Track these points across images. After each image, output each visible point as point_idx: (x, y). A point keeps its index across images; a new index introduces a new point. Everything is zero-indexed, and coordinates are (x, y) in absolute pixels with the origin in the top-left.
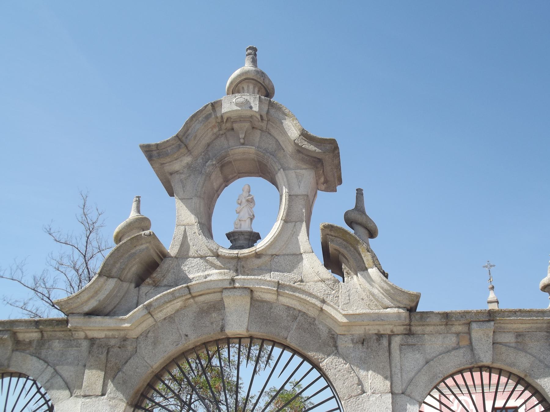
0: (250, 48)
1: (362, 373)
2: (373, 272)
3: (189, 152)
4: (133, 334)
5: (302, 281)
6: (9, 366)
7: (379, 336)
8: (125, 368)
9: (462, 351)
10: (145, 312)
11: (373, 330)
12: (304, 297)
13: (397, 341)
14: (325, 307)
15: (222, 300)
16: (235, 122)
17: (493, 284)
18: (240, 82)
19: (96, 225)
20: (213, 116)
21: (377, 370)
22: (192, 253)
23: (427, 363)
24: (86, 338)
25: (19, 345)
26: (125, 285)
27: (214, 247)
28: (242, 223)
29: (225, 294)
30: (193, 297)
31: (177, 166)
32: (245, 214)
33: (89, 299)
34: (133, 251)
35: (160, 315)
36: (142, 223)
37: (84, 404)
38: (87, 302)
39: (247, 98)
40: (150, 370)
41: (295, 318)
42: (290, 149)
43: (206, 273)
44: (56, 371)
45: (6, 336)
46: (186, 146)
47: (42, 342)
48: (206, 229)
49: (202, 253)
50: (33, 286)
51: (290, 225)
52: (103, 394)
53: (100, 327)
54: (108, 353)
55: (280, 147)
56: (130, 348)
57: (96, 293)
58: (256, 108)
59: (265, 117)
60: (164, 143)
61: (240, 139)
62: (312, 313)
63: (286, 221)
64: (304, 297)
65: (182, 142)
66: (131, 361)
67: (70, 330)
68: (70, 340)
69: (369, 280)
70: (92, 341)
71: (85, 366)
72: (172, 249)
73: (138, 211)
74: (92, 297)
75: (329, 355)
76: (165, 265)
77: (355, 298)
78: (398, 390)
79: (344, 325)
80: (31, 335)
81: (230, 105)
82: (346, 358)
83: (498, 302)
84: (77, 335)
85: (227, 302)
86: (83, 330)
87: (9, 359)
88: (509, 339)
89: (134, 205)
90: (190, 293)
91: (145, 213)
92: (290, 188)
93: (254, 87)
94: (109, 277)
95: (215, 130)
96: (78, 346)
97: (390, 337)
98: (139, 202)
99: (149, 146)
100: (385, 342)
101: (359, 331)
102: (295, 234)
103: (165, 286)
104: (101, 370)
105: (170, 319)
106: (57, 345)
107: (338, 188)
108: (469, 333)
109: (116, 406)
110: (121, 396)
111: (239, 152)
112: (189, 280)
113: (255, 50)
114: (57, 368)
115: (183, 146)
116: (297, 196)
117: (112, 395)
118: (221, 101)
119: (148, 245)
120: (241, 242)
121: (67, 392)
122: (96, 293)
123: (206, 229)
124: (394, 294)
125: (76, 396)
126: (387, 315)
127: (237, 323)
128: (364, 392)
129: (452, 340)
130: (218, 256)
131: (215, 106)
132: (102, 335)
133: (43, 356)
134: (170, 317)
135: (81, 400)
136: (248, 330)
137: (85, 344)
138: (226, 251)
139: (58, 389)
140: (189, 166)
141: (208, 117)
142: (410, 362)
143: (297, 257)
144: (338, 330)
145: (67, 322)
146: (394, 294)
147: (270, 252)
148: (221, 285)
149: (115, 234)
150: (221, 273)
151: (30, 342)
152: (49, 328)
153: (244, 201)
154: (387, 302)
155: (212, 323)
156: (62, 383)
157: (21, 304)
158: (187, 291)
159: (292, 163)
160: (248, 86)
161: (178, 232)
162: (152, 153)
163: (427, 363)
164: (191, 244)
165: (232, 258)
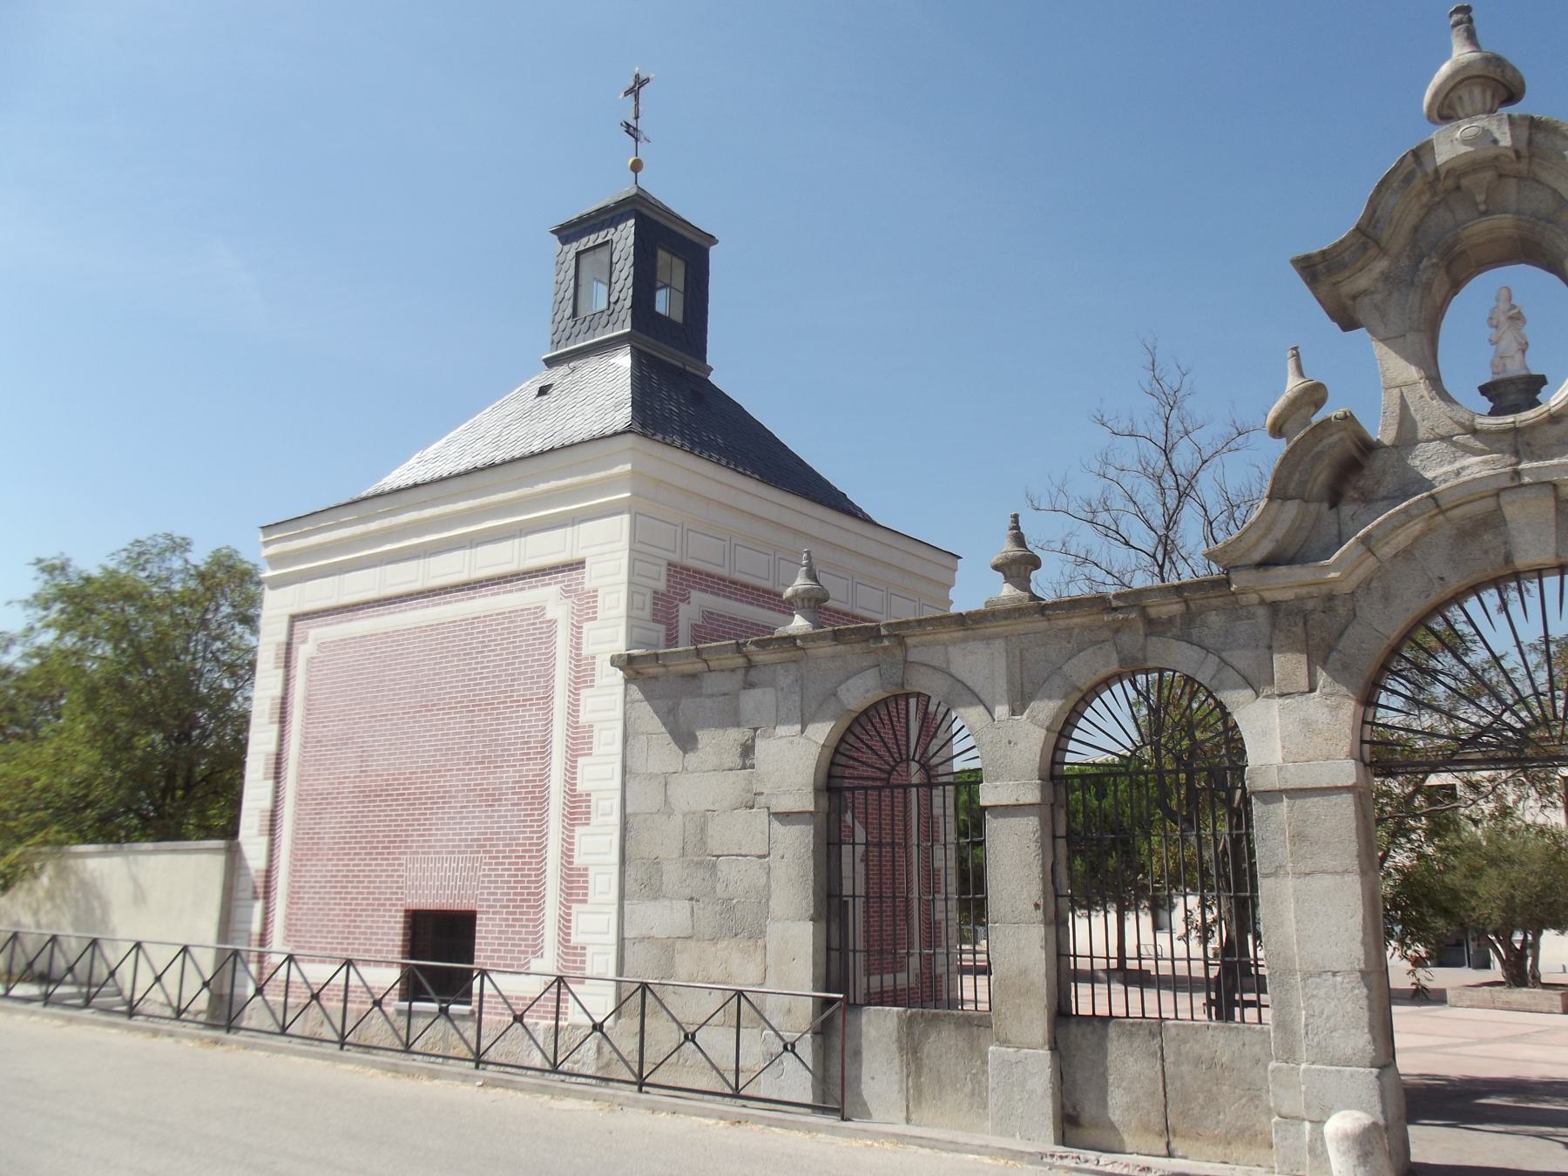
0: (1457, 11)
3: (1383, 251)
4: (1346, 587)
6: (1145, 660)
8: (1341, 646)
10: (1362, 548)
15: (1499, 507)
16: (1464, 174)
18: (1453, 88)
19: (1179, 394)
20: (1419, 174)
22: (1422, 433)
24: (1262, 602)
25: (1154, 626)
26: (1313, 507)
27: (1464, 417)
28: (1508, 361)
31: (1363, 282)
32: (1509, 342)
33: (1258, 542)
34: (1319, 448)
35: (1386, 551)
36: (1314, 395)
37: (1282, 708)
39: (1483, 122)
40: (1387, 642)
43: (1457, 465)
45: (1133, 615)
46: (1377, 243)
47: (1189, 618)
49: (1442, 431)
52: (1312, 690)
53: (1285, 583)
54: (1305, 624)
56: (1342, 611)
57: (1269, 529)
58: (1505, 140)
59: (1525, 153)
60: (1335, 246)
61: (1477, 204)
65: (1368, 236)
66: (1350, 631)
67: (1233, 594)
68: (1235, 609)
70: (1274, 607)
71: (1270, 647)
72: (1382, 431)
73: (1300, 372)
74: (1263, 536)
76: (1378, 462)
80: (1170, 608)
81: (1451, 144)
84: (1244, 599)
85: (1509, 511)
86: (1255, 592)
87: (1144, 648)
89: (1291, 365)
90: (1438, 506)
93: (1484, 91)
95: (1425, 198)
98: (1297, 356)
99: (1307, 258)
103: (1384, 498)
104: (1300, 652)
105: (1406, 553)
106: (1214, 619)
109: (1338, 707)
110: (1344, 690)
112: (1428, 484)
113: (1466, 10)
114: (1224, 655)
115: (1371, 244)
117: (1328, 690)
119: (1342, 434)
120: (1512, 398)
121: (1250, 692)
122: (1269, 529)
125: (1267, 697)
130: (1474, 432)
131: (1420, 154)
132: (1289, 595)
133: (1195, 638)
134: (1405, 551)
135: (1276, 703)
136: (1557, 556)
137: (1262, 612)
139: (1234, 688)
140: (1385, 277)
141: (1408, 179)
145: (1228, 582)
148: (1495, 485)
149: (1269, 421)
150: (1485, 462)
151: (1171, 620)
153: (1503, 318)
155: (1486, 552)
158: (1431, 503)
160: (1471, 92)
161: (1389, 401)
162: (1312, 269)
164: (1418, 418)
165: (1504, 432)
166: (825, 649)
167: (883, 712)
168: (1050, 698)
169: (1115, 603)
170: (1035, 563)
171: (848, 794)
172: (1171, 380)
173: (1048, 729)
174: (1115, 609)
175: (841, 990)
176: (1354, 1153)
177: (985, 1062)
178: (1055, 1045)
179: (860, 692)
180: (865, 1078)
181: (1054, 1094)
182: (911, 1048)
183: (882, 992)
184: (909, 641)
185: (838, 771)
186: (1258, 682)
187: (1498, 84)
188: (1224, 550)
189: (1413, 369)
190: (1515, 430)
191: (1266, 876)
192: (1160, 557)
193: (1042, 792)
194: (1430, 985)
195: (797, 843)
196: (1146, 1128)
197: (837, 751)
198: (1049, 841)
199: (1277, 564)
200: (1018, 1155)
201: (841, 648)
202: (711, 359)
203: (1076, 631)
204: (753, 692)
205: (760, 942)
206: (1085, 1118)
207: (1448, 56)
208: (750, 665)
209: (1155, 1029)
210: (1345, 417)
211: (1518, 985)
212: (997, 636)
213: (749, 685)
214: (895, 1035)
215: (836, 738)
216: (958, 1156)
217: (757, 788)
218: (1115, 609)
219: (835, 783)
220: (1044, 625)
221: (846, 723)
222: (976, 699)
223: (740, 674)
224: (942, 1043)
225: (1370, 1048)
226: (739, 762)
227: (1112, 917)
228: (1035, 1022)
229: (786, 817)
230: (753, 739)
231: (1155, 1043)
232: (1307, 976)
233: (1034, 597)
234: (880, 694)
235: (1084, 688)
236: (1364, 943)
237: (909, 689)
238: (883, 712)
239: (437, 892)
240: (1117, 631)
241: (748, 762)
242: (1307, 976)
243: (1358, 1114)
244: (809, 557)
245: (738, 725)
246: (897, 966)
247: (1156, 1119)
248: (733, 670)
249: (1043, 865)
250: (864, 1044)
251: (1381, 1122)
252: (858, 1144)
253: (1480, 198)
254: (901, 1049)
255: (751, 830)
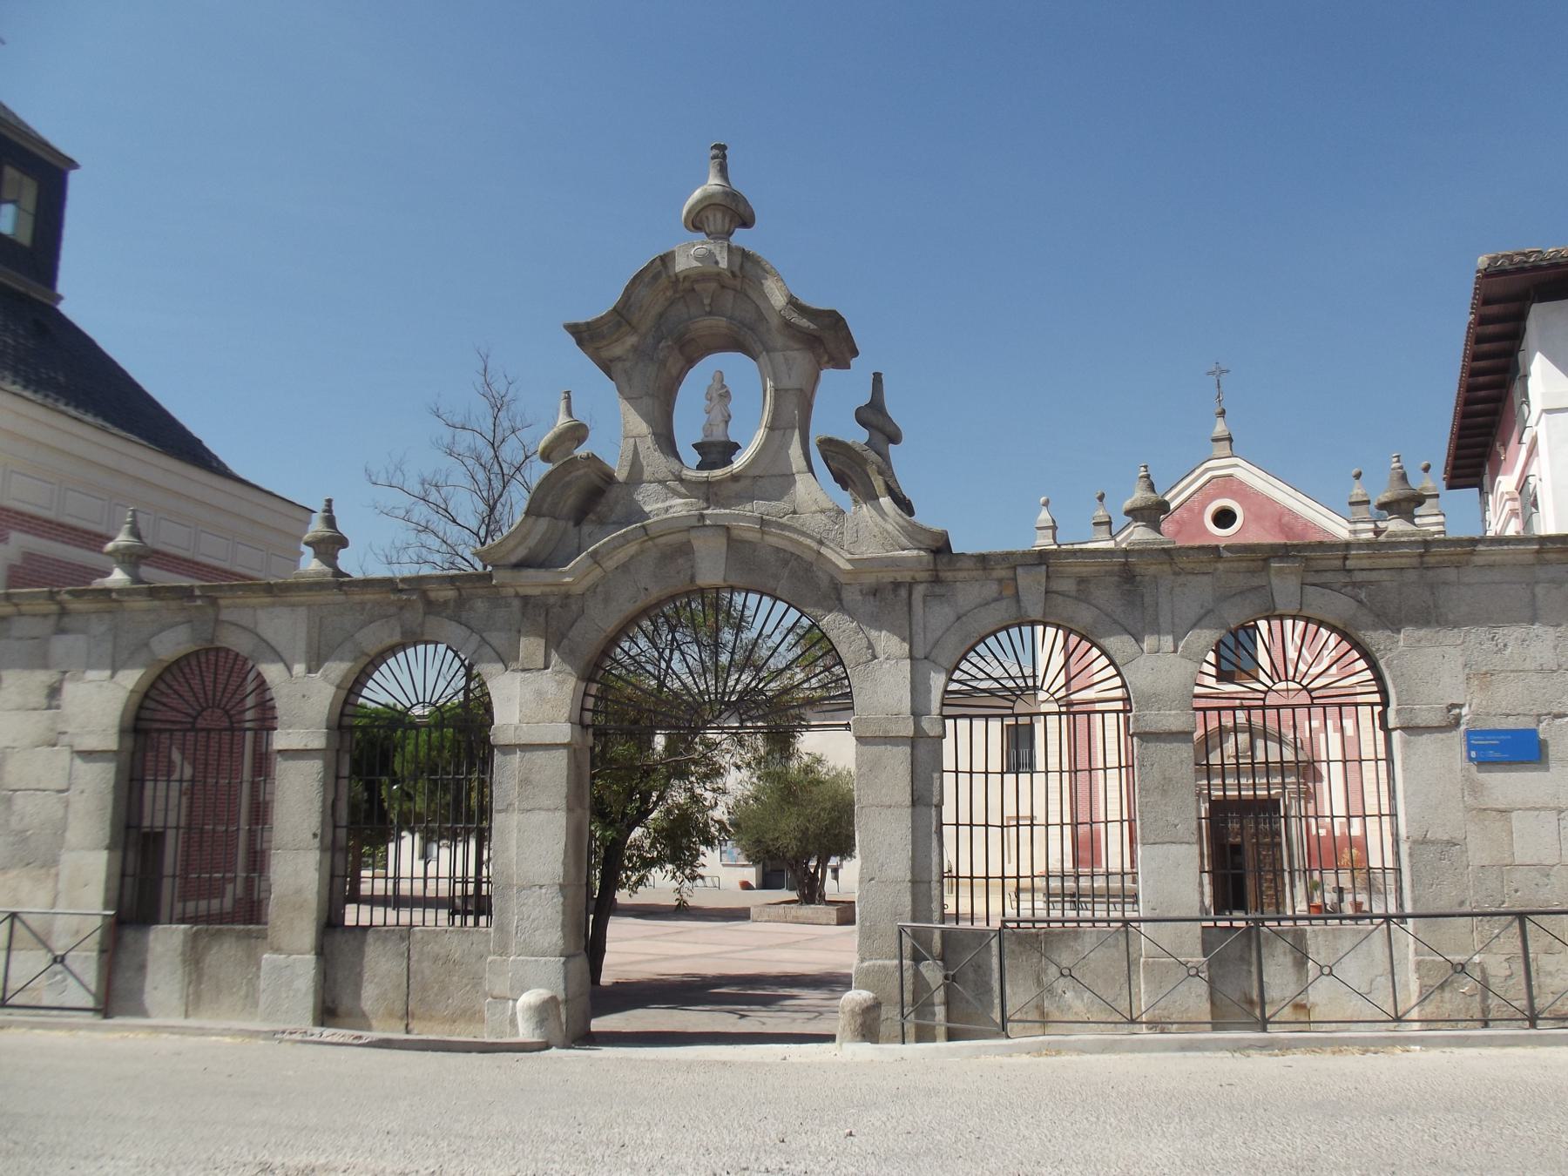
0: (715, 147)
1: (874, 634)
2: (885, 501)
4: (578, 590)
5: (794, 512)
7: (896, 585)
8: (570, 634)
9: (1004, 603)
10: (590, 561)
11: (888, 577)
12: (795, 536)
13: (919, 591)
14: (823, 550)
16: (697, 281)
17: (1224, 405)
21: (893, 630)
23: (959, 618)
24: (517, 595)
25: (431, 606)
26: (561, 524)
29: (693, 534)
30: (652, 539)
31: (617, 350)
32: (717, 415)
33: (516, 547)
35: (610, 564)
36: (577, 433)
37: (523, 680)
38: (513, 550)
41: (786, 563)
42: (775, 322)
43: (668, 504)
44: (483, 638)
47: (461, 602)
48: (666, 442)
49: (660, 478)
50: (422, 494)
51: (778, 433)
52: (546, 667)
53: (534, 582)
55: (761, 317)
57: (524, 538)
58: (724, 264)
60: (597, 320)
62: (809, 556)
63: (772, 428)
64: (795, 536)
68: (497, 599)
69: (881, 511)
70: (526, 600)
72: (621, 474)
73: (569, 413)
74: (519, 544)
75: (830, 611)
76: (613, 493)
77: (864, 534)
78: (919, 654)
79: (848, 572)
82: (853, 616)
83: (1230, 439)
85: (698, 544)
87: (422, 625)
88: (1068, 586)
89: (563, 405)
91: (580, 415)
92: (775, 380)
94: (539, 515)
95: (669, 294)
96: (508, 605)
97: (911, 586)
98: (568, 399)
100: (903, 593)
101: (869, 579)
102: (786, 446)
105: (624, 567)
106: (480, 606)
107: (853, 362)
108: (1015, 579)
109: (564, 682)
110: (569, 669)
111: (705, 324)
112: (646, 516)
116: (786, 390)
118: (673, 252)
121: (500, 666)
122: (524, 538)
123: (666, 442)
124: (915, 534)
126: (904, 559)
127: (710, 570)
128: (875, 657)
129: (992, 589)
130: (681, 480)
131: (666, 259)
132: (537, 591)
135: (519, 675)
137: (516, 603)
138: (691, 474)
140: (635, 349)
141: (656, 277)
142: (938, 617)
143: (788, 479)
144: (842, 579)
145: (490, 576)
146: (915, 534)
147: (751, 473)
149: (542, 444)
151: (446, 603)
152: (468, 585)
154: (904, 541)
156: (493, 654)
157: (403, 513)
159: (779, 340)
162: (584, 335)
163: (959, 618)
165: (700, 483)
166: (142, 603)
167: (194, 662)
168: (341, 660)
169: (400, 586)
170: (342, 542)
171: (155, 735)
172: (499, 386)
173: (338, 687)
174: (401, 591)
175: (133, 909)
176: (534, 1020)
177: (259, 968)
178: (321, 951)
179: (172, 643)
180: (148, 987)
181: (316, 991)
182: (193, 959)
183: (209, 915)
184: (222, 602)
185: (146, 714)
186: (506, 659)
187: (731, 212)
188: (488, 551)
189: (645, 425)
190: (708, 483)
191: (499, 811)
192: (482, 533)
193: (328, 739)
194: (691, 902)
195: (97, 782)
196: (391, 1014)
197: (146, 696)
198: (332, 781)
199: (529, 566)
200: (255, 1034)
201: (157, 603)
202: (62, 287)
203: (369, 606)
204: (64, 637)
205: (53, 871)
206: (342, 1009)
207: (705, 182)
208: (63, 612)
209: (405, 934)
210: (588, 457)
211: (808, 903)
212: (301, 604)
213: (61, 631)
214: (180, 950)
215: (146, 685)
216: (203, 1038)
217: (61, 727)
218: (401, 591)
219: (141, 726)
220: (341, 598)
221: (157, 671)
222: (278, 657)
223: (52, 621)
224: (224, 953)
225: (561, 942)
226: (44, 702)
227: (473, 844)
228: (306, 932)
229: (88, 755)
230: (61, 681)
231: (404, 946)
232: (522, 888)
233: (338, 573)
234: (192, 648)
235: (372, 653)
236: (564, 864)
237: (218, 644)
238: (194, 662)
239: (1559, 737)
240: (401, 608)
241: (55, 703)
242: (522, 888)
243: (542, 991)
244: (134, 516)
245: (46, 667)
246: (215, 890)
247: (399, 1006)
248: (45, 616)
249: (324, 801)
250: (150, 958)
251: (561, 996)
252: (111, 1036)
253: (707, 301)
254: (184, 961)
255: (53, 766)
